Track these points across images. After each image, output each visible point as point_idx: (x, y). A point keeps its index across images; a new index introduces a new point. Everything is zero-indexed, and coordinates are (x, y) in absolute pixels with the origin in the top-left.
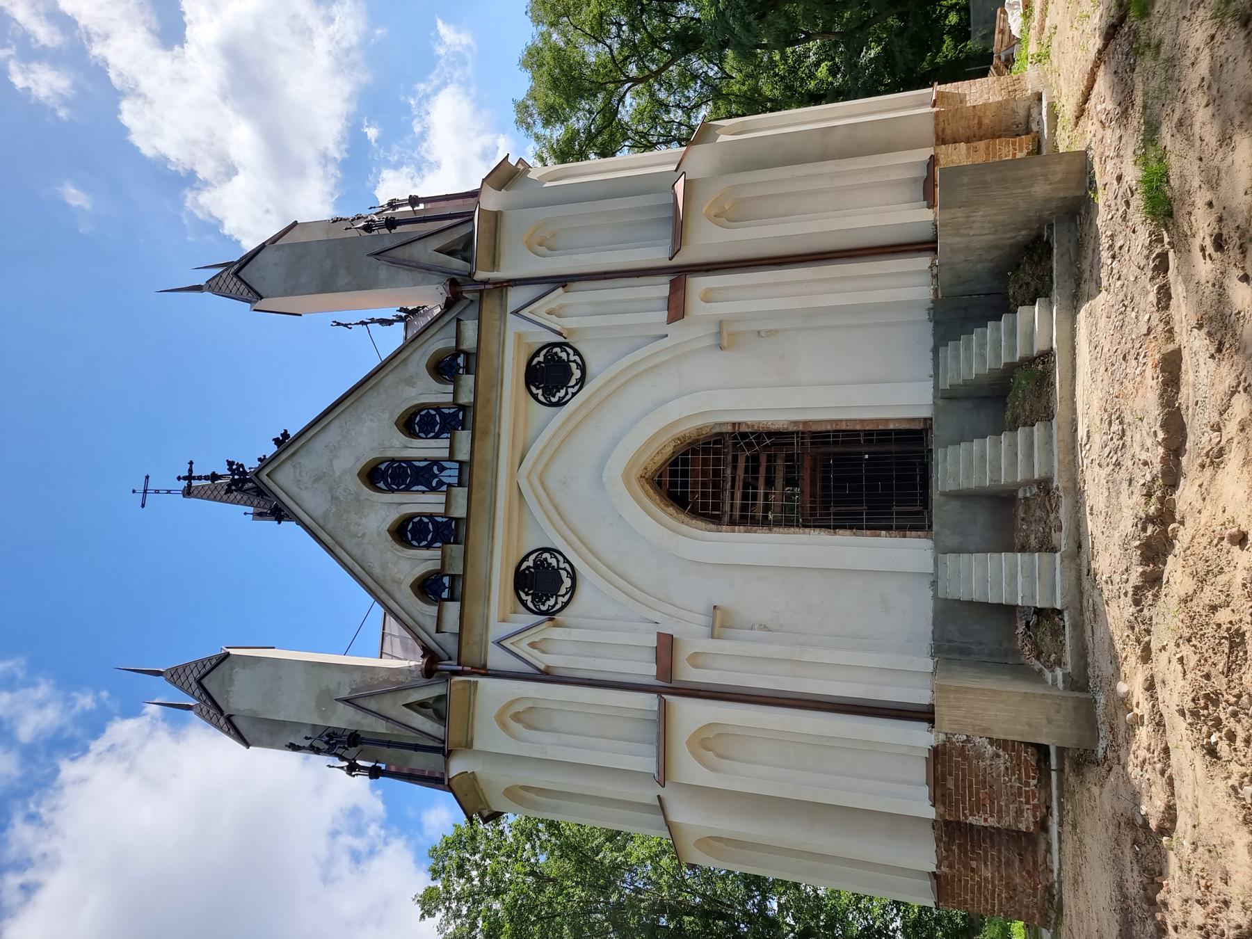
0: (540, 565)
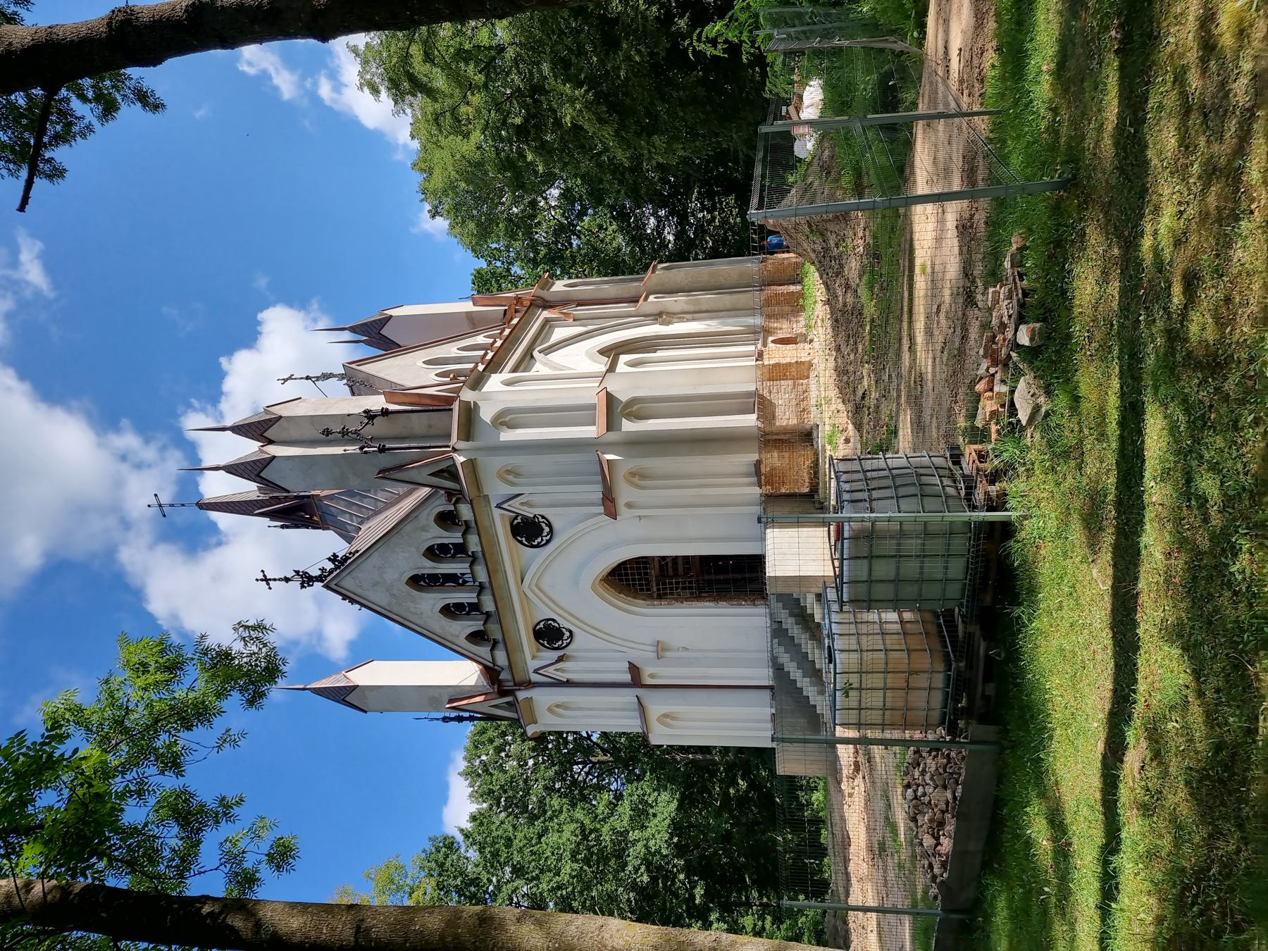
0: (548, 627)
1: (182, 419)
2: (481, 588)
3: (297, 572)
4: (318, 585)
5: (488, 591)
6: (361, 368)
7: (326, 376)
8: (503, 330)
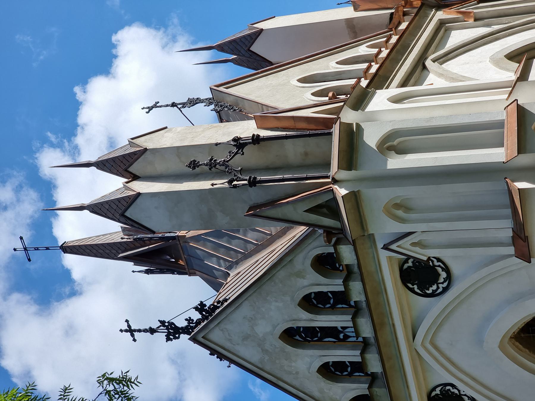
1: (37, 155)
2: (365, 346)
3: (163, 323)
4: (184, 338)
5: (374, 349)
6: (231, 91)
7: (193, 102)
8: (389, 38)
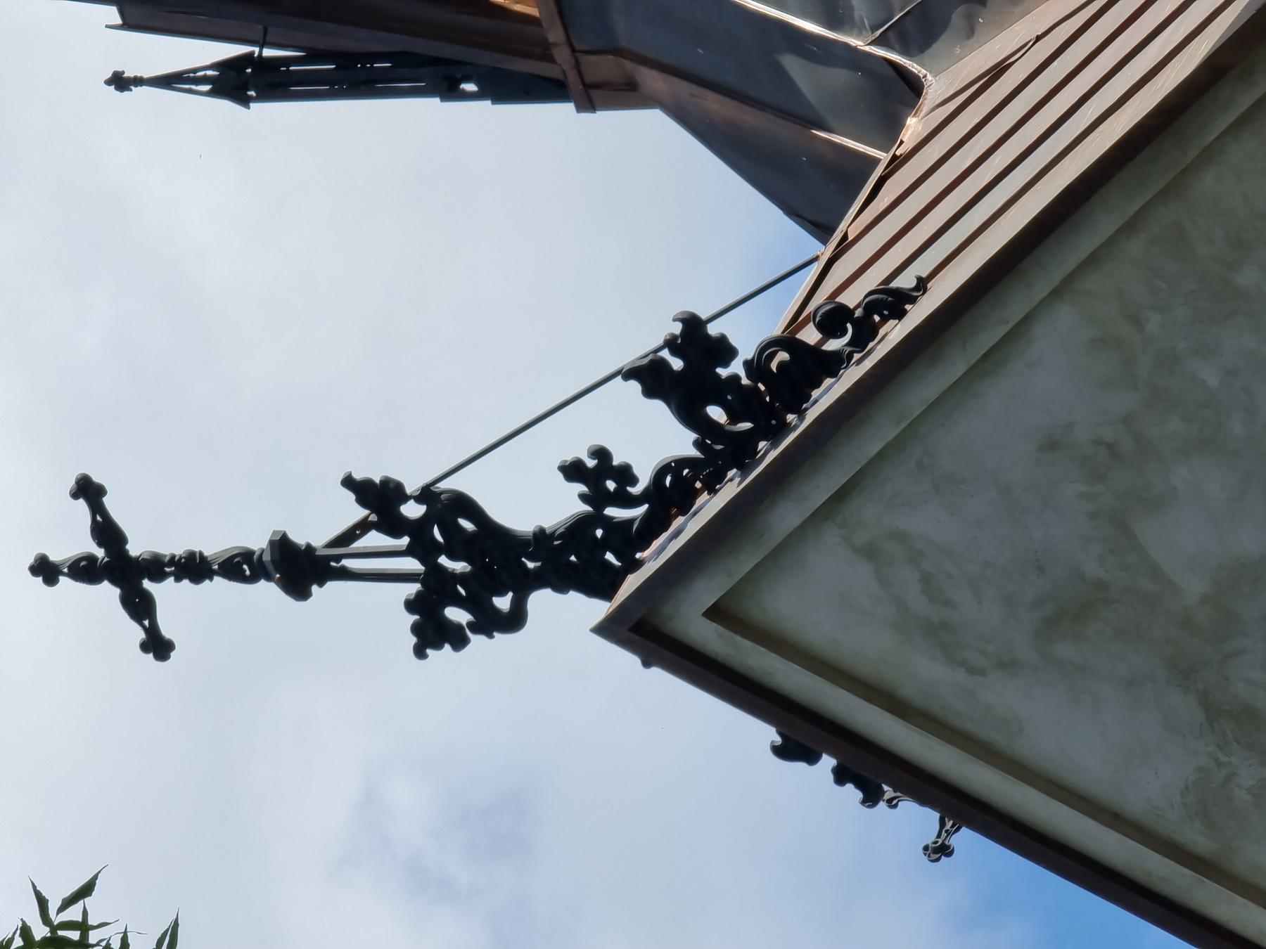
3: (380, 498)
4: (563, 619)
